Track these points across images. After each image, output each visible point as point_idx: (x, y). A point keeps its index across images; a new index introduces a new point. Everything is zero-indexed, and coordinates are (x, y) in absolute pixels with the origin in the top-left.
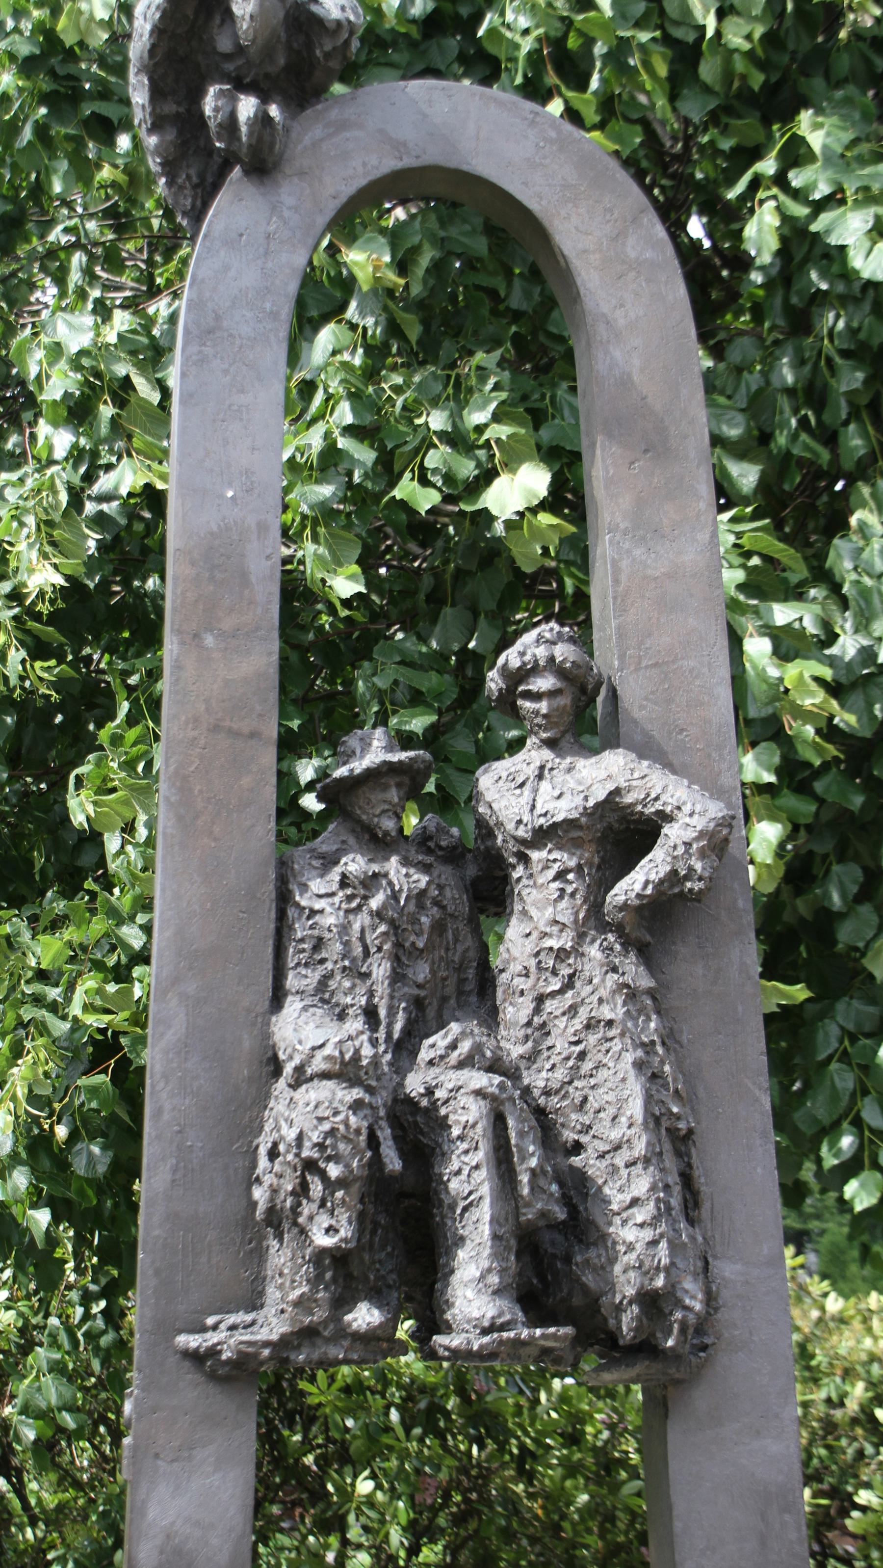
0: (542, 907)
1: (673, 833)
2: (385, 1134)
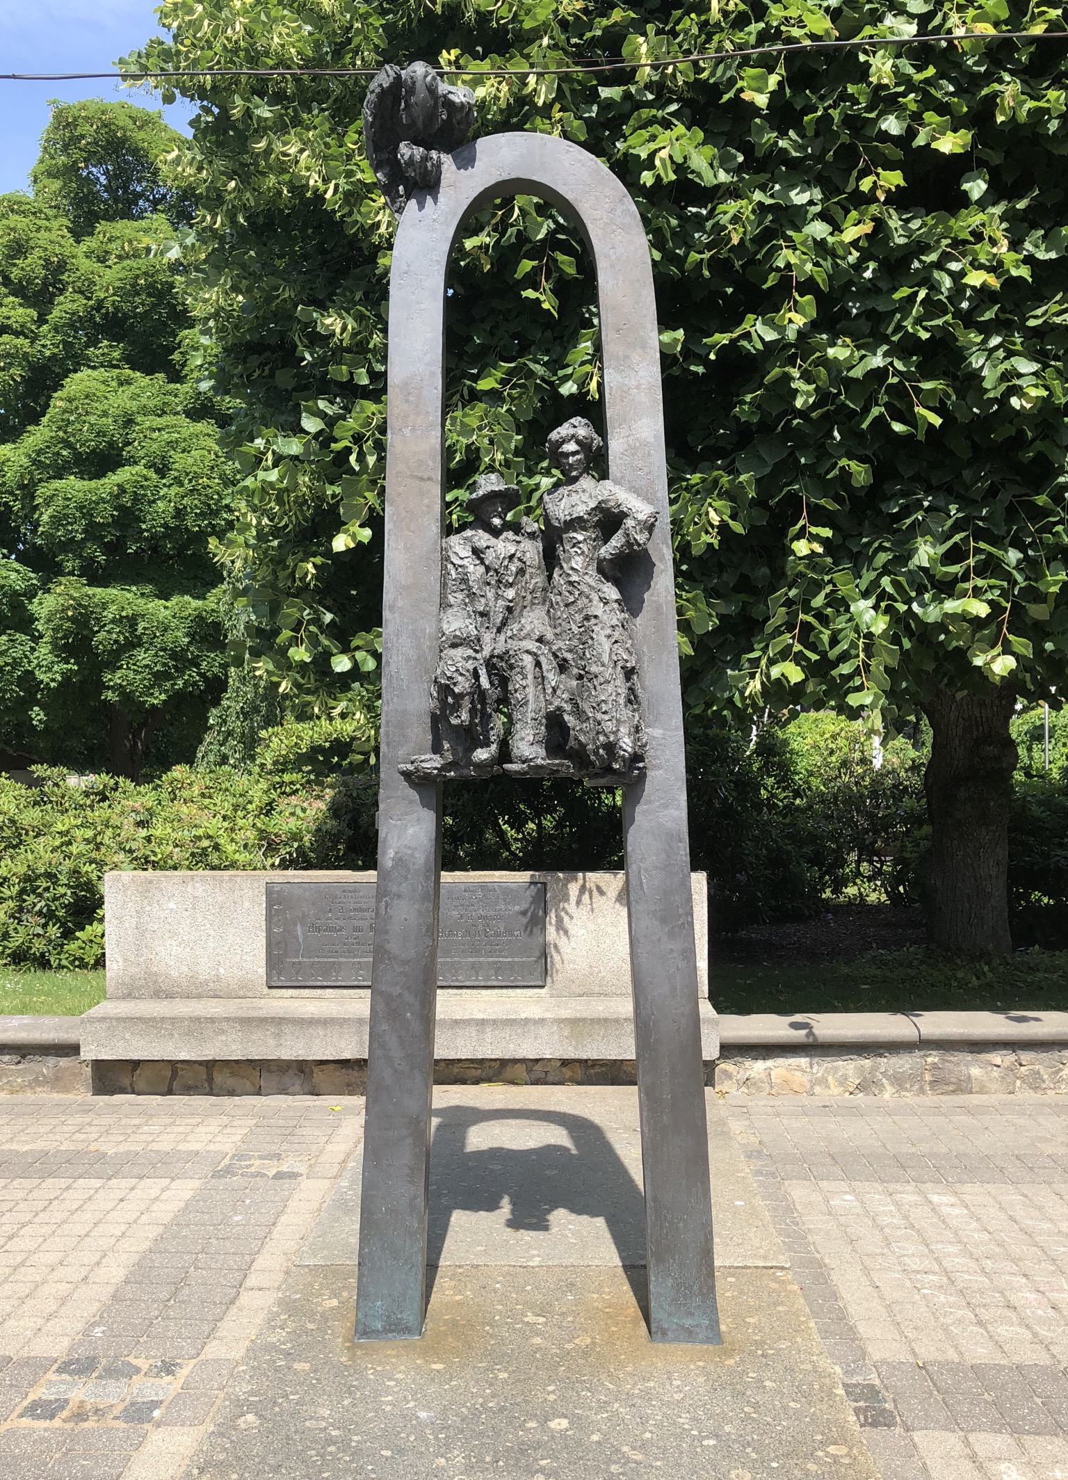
0: (579, 559)
1: (629, 523)
2: (483, 673)
